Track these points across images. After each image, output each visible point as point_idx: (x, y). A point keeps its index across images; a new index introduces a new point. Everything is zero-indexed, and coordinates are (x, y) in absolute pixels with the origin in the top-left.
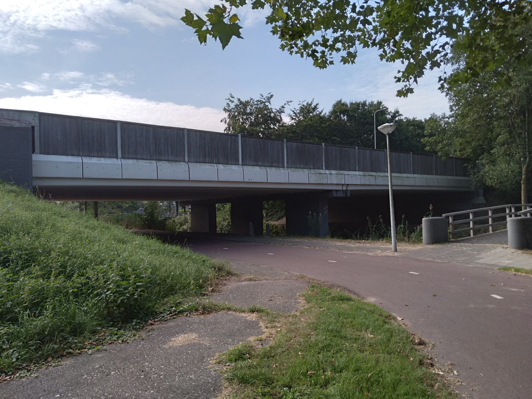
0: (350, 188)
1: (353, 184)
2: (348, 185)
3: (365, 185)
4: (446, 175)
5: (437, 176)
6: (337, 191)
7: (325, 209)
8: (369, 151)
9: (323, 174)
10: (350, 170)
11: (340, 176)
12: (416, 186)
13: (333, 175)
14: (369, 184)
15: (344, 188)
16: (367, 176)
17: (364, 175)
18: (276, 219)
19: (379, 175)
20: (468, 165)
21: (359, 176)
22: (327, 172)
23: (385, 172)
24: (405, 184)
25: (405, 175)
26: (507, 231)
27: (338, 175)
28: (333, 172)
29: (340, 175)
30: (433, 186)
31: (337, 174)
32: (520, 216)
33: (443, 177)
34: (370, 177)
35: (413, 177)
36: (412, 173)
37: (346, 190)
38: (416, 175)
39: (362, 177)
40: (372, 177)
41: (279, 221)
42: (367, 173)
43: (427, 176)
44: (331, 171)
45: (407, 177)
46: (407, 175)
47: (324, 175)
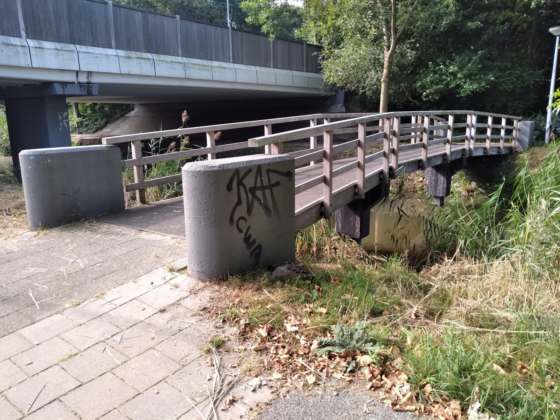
0: (95, 79)
1: (100, 71)
2: (90, 73)
3: (129, 75)
4: (290, 70)
5: (275, 69)
6: (64, 84)
7: (60, 117)
8: (140, 13)
9: (17, 45)
10: (95, 45)
11: (67, 55)
12: (213, 81)
13: (45, 50)
14: (140, 74)
15: (83, 79)
16: (135, 59)
17: (128, 58)
18: (92, 131)
19: (163, 59)
20: (318, 54)
21: (115, 58)
22: (32, 43)
23: (178, 56)
24: (216, 78)
25: (215, 64)
26: (182, 202)
27: (61, 52)
28: (48, 45)
29: (64, 53)
30: (110, 73)
31: (56, 49)
32: (260, 150)
33: (285, 72)
34: (142, 61)
35: (233, 69)
36: (231, 60)
37: (88, 83)
38: (237, 66)
39: (122, 60)
40: (147, 61)
41: (96, 133)
42: (133, 54)
43: (258, 68)
44: (42, 42)
45: (221, 67)
46: (222, 63)
47: (20, 49)
